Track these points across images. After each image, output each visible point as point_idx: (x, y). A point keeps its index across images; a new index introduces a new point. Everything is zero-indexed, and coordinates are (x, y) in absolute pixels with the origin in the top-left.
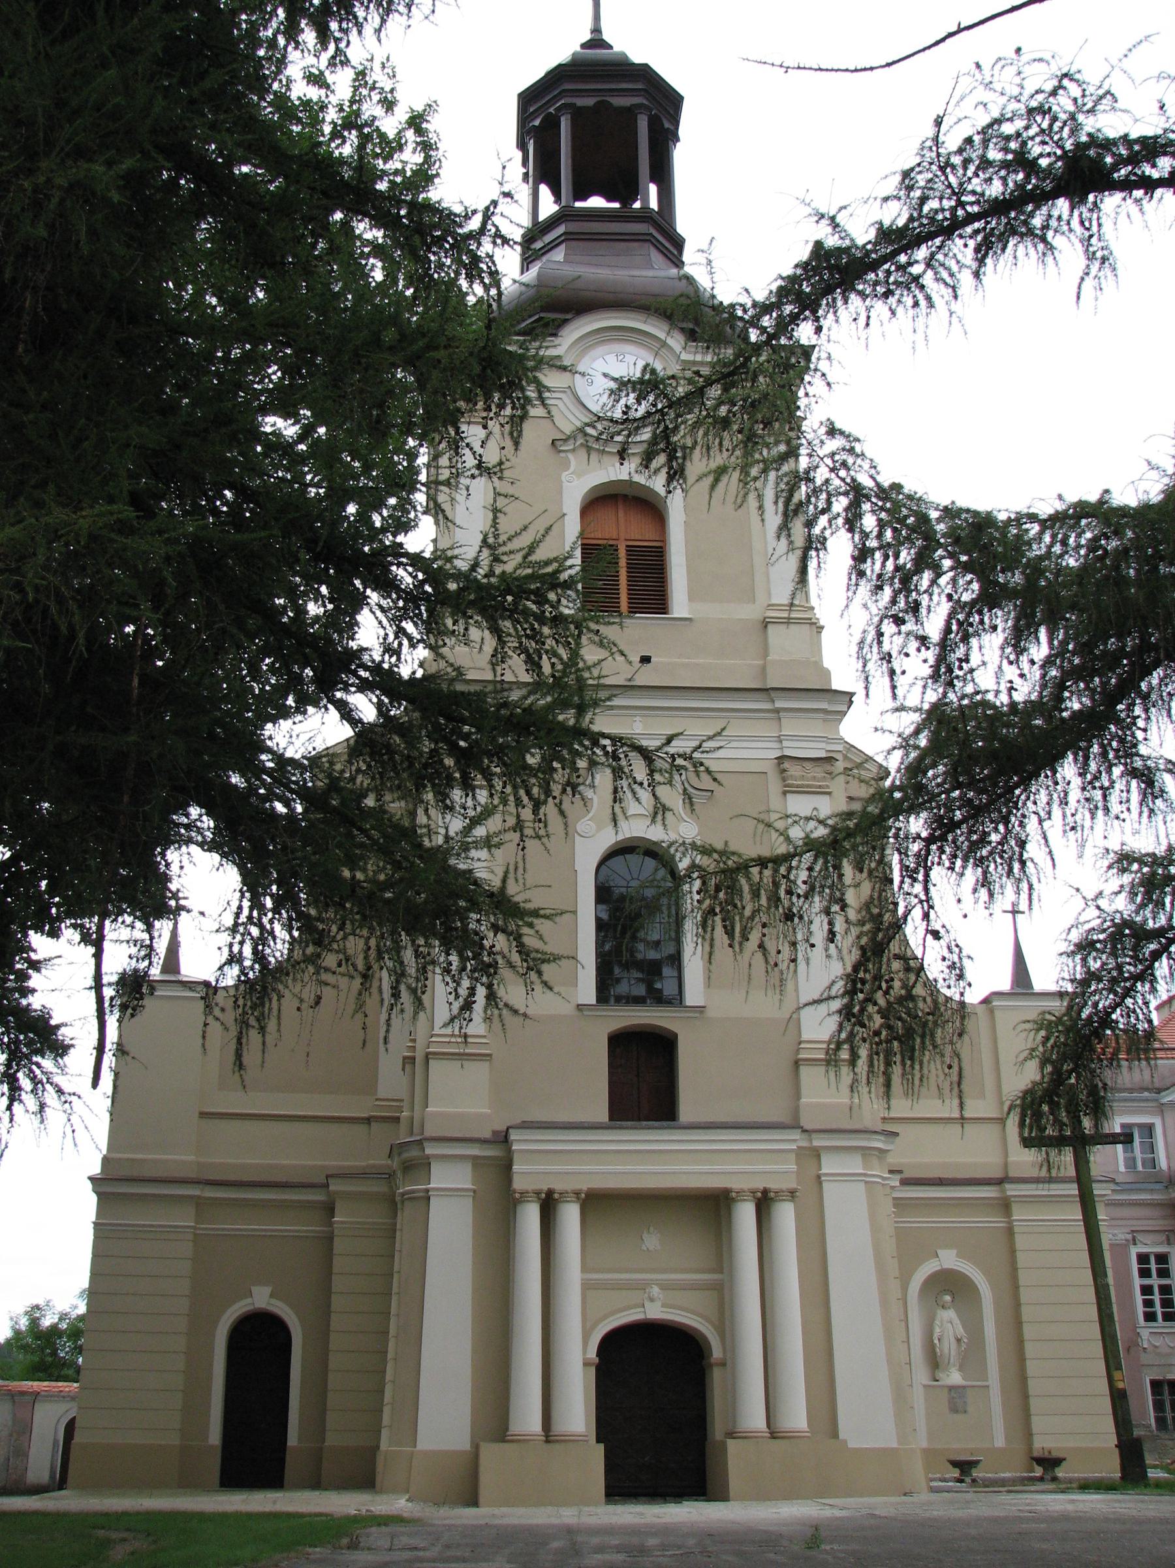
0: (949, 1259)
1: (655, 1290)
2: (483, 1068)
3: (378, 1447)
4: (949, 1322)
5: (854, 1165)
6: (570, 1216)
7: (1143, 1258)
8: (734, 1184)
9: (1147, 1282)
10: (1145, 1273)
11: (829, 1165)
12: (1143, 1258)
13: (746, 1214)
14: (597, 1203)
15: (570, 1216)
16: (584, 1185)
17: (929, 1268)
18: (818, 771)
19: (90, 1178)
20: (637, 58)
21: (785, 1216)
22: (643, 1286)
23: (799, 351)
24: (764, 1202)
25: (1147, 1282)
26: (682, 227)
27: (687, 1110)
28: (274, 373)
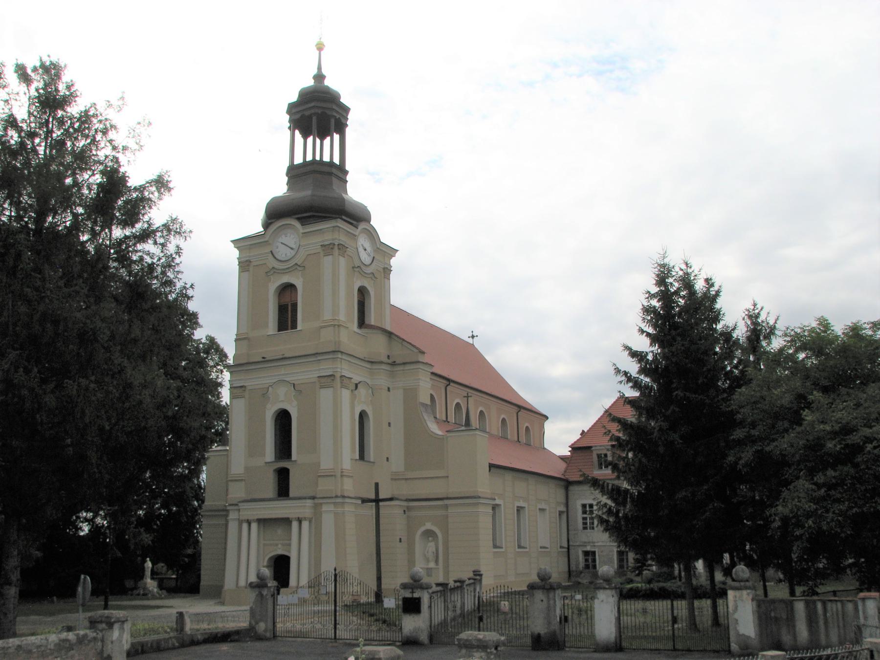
0: (429, 526)
1: (280, 546)
2: (242, 484)
3: (222, 587)
4: (431, 546)
5: (331, 508)
6: (254, 526)
7: (584, 506)
8: (290, 516)
9: (585, 516)
10: (584, 512)
11: (325, 508)
12: (584, 506)
13: (295, 525)
14: (259, 521)
15: (254, 526)
16: (256, 517)
17: (423, 529)
18: (329, 380)
20: (286, 179)
21: (305, 525)
22: (277, 545)
23: (292, 239)
24: (300, 521)
25: (585, 516)
26: (347, 168)
27: (291, 494)
28: (80, 309)
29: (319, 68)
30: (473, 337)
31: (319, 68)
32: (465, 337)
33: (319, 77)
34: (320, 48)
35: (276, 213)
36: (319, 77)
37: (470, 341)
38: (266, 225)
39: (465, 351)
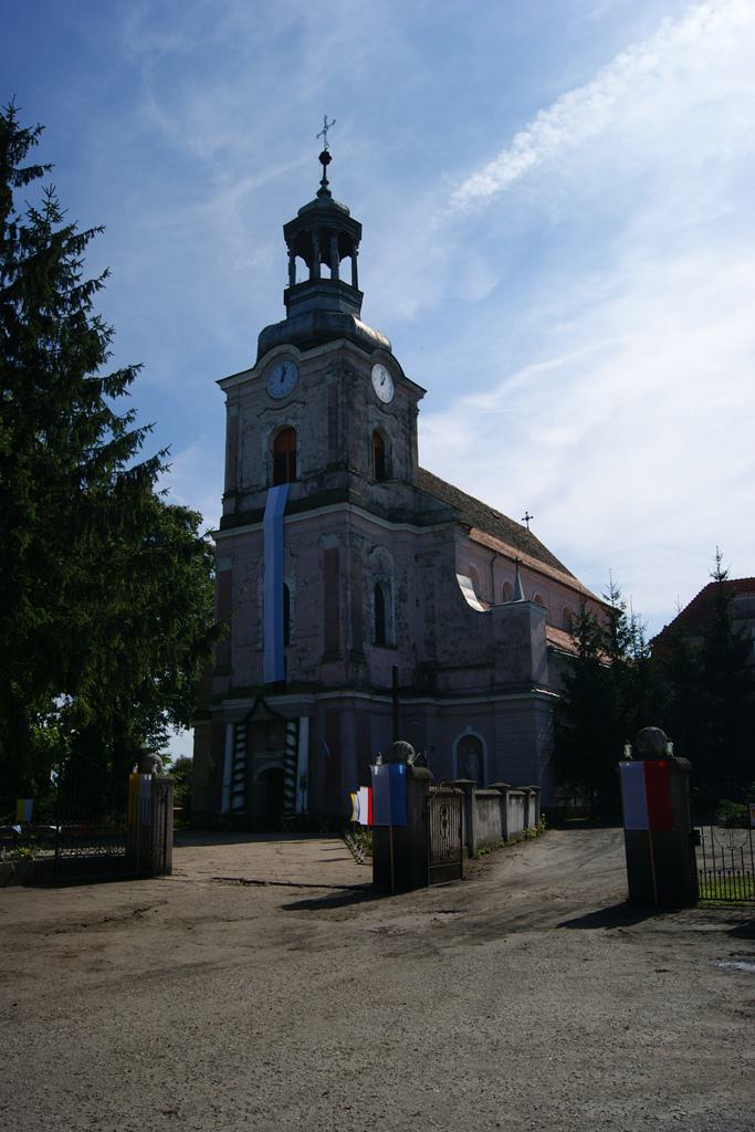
0: (469, 731)
19: (218, 382)
29: (324, 182)
30: (527, 519)
31: (324, 182)
32: (518, 520)
33: (324, 193)
34: (325, 158)
35: (270, 340)
36: (324, 193)
37: (524, 524)
38: (261, 353)
39: (520, 536)
